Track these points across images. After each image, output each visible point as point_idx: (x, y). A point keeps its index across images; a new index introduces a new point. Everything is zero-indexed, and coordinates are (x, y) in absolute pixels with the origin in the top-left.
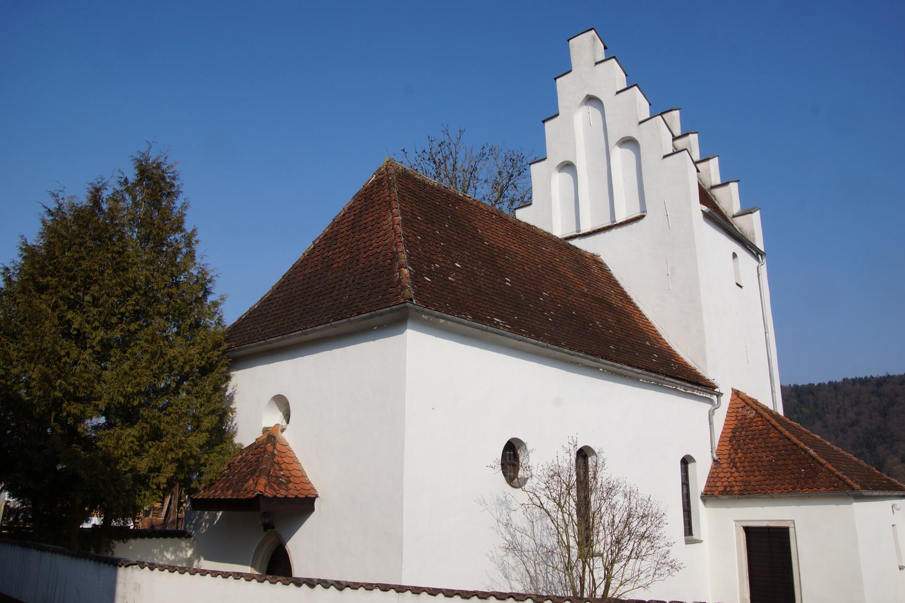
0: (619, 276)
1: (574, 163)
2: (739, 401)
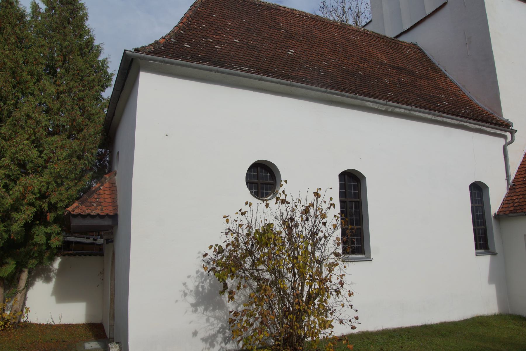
0: (431, 55)
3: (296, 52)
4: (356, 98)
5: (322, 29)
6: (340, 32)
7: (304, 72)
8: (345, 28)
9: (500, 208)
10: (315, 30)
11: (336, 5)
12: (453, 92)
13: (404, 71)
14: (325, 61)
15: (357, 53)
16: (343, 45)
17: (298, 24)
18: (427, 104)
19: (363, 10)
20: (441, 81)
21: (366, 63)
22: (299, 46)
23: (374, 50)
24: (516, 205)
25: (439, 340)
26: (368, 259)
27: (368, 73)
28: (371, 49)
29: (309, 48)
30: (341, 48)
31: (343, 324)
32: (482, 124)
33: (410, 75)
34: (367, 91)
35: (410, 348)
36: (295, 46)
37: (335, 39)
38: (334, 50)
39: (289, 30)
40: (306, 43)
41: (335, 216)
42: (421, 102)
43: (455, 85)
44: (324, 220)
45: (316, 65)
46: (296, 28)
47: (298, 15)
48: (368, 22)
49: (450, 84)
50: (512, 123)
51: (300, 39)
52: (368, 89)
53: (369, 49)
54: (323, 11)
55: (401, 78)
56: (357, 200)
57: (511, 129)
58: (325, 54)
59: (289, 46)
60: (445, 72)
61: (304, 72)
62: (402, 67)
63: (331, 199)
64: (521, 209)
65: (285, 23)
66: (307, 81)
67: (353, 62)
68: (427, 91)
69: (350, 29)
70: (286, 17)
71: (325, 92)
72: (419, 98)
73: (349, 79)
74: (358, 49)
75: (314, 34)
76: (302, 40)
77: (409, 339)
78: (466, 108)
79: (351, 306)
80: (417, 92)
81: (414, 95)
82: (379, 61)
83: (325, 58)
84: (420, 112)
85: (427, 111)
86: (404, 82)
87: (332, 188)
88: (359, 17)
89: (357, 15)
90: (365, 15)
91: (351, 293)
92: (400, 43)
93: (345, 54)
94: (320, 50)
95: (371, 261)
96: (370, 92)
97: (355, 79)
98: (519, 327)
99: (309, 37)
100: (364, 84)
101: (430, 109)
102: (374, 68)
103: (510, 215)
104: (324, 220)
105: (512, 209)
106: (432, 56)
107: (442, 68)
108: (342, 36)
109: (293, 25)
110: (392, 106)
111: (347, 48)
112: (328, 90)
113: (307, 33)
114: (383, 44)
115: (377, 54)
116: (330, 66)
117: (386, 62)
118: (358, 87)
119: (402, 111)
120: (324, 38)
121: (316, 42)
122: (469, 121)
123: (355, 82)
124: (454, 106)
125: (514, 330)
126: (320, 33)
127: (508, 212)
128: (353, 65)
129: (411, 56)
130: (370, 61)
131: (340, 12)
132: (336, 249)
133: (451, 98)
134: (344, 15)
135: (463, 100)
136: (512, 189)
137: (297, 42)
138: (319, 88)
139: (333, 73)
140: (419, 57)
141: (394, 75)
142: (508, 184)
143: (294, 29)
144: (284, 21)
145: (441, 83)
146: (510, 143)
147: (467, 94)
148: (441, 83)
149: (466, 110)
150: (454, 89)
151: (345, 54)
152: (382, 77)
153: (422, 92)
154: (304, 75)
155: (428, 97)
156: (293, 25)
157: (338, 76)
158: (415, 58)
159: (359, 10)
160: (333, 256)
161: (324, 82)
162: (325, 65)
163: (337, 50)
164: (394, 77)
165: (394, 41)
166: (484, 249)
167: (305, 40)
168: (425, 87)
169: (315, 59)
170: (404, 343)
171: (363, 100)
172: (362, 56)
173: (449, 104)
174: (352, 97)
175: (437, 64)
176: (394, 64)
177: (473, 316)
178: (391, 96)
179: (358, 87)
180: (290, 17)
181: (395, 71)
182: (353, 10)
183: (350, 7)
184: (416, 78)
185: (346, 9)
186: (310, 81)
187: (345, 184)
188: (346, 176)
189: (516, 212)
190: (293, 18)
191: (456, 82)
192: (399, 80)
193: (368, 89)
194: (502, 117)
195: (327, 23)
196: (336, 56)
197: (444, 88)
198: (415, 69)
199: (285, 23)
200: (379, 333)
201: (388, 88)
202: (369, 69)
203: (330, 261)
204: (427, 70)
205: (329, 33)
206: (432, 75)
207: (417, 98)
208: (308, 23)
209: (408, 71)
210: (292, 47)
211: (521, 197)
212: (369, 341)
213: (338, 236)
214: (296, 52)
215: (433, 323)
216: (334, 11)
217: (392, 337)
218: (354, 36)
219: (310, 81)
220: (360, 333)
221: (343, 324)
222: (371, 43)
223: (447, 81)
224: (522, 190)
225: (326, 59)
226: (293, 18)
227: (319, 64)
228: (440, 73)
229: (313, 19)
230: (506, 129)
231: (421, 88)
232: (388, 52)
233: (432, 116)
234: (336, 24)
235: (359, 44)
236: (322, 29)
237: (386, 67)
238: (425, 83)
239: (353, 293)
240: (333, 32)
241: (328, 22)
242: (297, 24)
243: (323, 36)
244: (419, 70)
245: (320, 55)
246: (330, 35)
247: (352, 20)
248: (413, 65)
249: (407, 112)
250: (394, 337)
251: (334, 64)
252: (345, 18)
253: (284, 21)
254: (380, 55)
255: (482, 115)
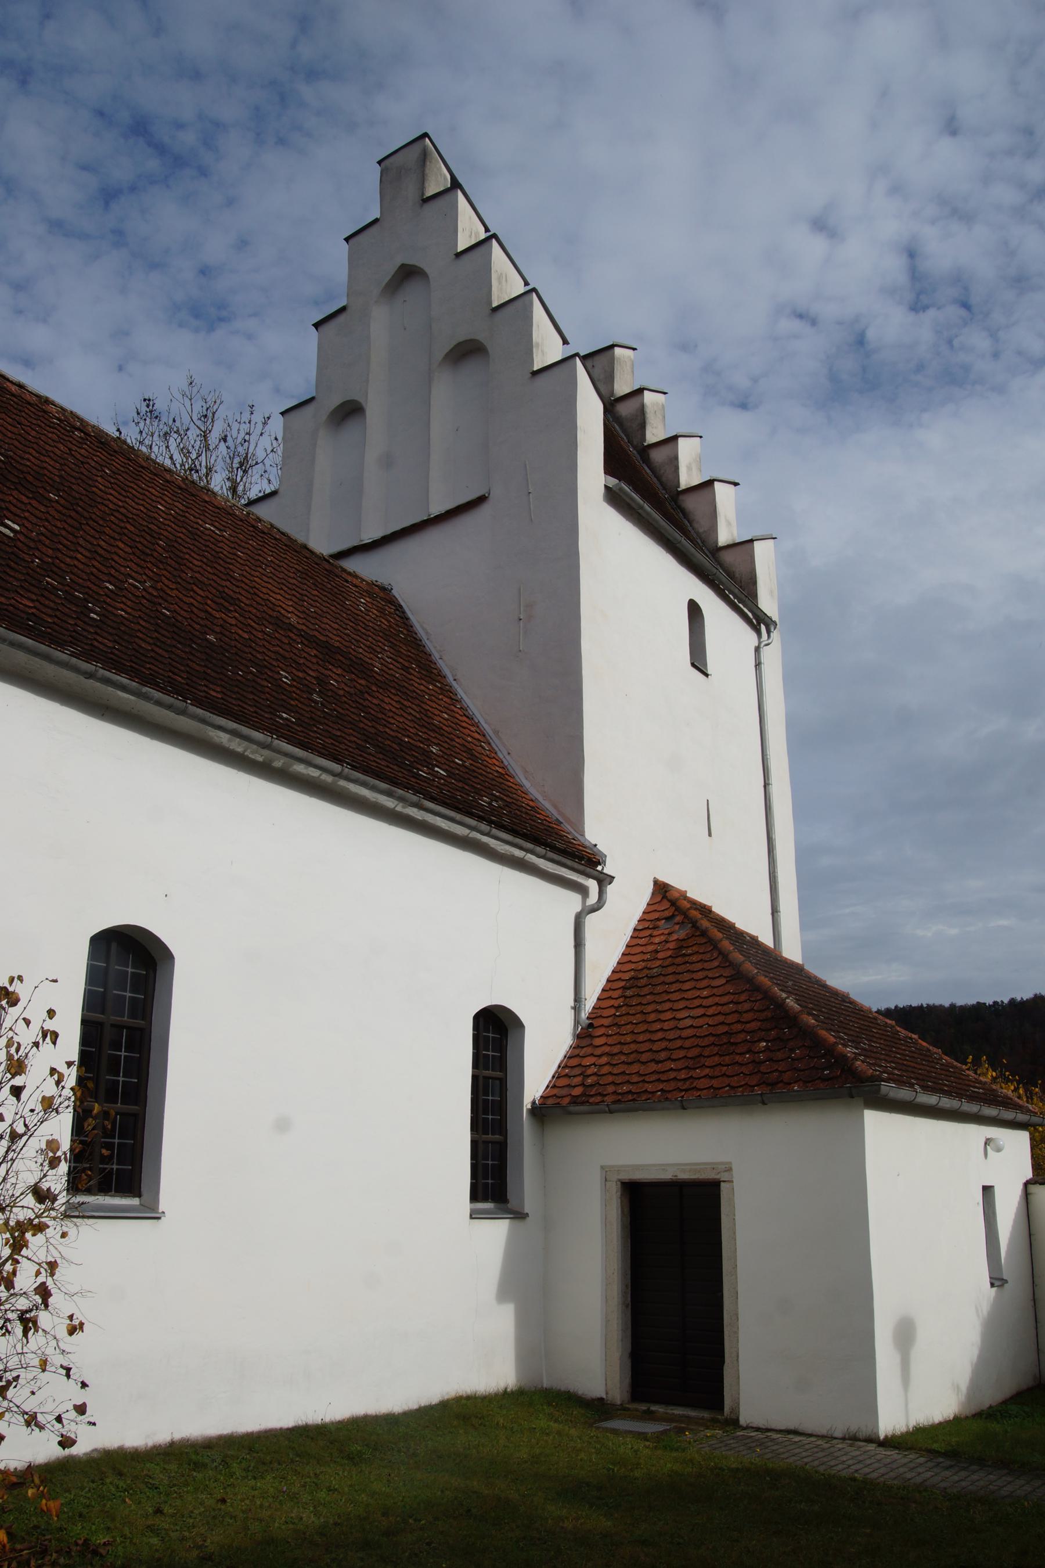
0: (424, 629)
1: (364, 404)
2: (666, 904)
3: (24, 531)
4: (183, 712)
5: (122, 480)
6: (176, 504)
7: (38, 601)
8: (193, 495)
9: (548, 1086)
10: (99, 479)
11: (186, 420)
12: (466, 744)
13: (341, 658)
14: (111, 579)
15: (215, 578)
16: (176, 545)
17: (50, 449)
18: (388, 767)
19: (260, 455)
20: (440, 708)
21: (235, 611)
22: (40, 515)
23: (265, 579)
24: (589, 1081)
25: (341, 1473)
26: (151, 1212)
27: (233, 643)
28: (257, 574)
29: (70, 529)
30: (167, 551)
31: (37, 1425)
32: (530, 846)
33: (356, 672)
34: (220, 696)
35: (247, 1502)
36: (27, 514)
37: (155, 522)
38: (147, 555)
39: (18, 459)
40: (64, 511)
41: (53, 1071)
42: (372, 758)
43: (473, 725)
44: (18, 1081)
45: (79, 584)
46: (42, 458)
47: (58, 419)
48: (268, 491)
49: (460, 718)
50: (606, 856)
51: (46, 495)
52: (225, 690)
53: (253, 573)
54: (142, 425)
55: (327, 676)
56: (140, 1023)
57: (601, 872)
58: (116, 558)
59: (7, 509)
60: (454, 684)
61: (38, 601)
62: (337, 644)
63: (51, 1013)
64: (600, 1094)
65: (9, 435)
66: (42, 631)
67: (195, 602)
68: (394, 727)
69: (206, 502)
70: (17, 418)
71: (90, 675)
72: (369, 744)
73: (174, 649)
74: (219, 567)
75: (94, 489)
76: (50, 500)
77: (250, 1474)
78: (493, 795)
79: (68, 1370)
80: (367, 725)
81: (355, 733)
82: (275, 614)
83: (113, 571)
84: (364, 784)
85: (384, 786)
86: (335, 690)
87: (55, 981)
88: (245, 472)
89: (241, 464)
90: (265, 471)
91: (76, 1322)
92: (344, 575)
93: (175, 573)
94: (102, 543)
95: (159, 1218)
96: (230, 700)
97: (191, 653)
98: (561, 1426)
99: (77, 496)
100: (213, 674)
101: (394, 782)
102: (255, 632)
103: (572, 1108)
104: (18, 1081)
105: (577, 1091)
106: (427, 633)
107: (446, 671)
108: (179, 517)
109: (35, 446)
110: (286, 755)
111: (187, 556)
112: (101, 671)
113: (74, 481)
114: (296, 566)
115: (271, 594)
116: (124, 599)
117: (294, 620)
118: (194, 679)
119: (314, 773)
120: (122, 510)
121: (94, 516)
122: (495, 831)
123: (190, 664)
124: (460, 784)
125: (547, 1434)
126: (113, 492)
127: (567, 1100)
128: (195, 610)
129: (368, 618)
130: (246, 608)
131: (192, 442)
132: (45, 1176)
133: (457, 760)
134: (204, 454)
135: (489, 770)
136: (584, 1036)
137: (34, 502)
138: (74, 660)
139: (127, 623)
140: (390, 626)
141: (310, 665)
142: (577, 1021)
143: (33, 460)
144: (9, 427)
145: (437, 712)
146: (594, 909)
147: (501, 756)
148: (437, 712)
149: (492, 801)
150: (469, 735)
151: (175, 573)
152: (274, 663)
153: (381, 728)
154: (34, 607)
155: (395, 746)
156: (35, 446)
157: (141, 635)
158: (377, 628)
159: (251, 450)
160: (30, 1200)
161: (92, 645)
162: (109, 593)
163: (155, 554)
164: (308, 670)
165: (327, 566)
166: (494, 1200)
167: (62, 502)
168: (391, 714)
169: (81, 566)
170: (233, 1485)
171: (204, 721)
172: (226, 590)
173: (450, 774)
174: (170, 707)
175: (436, 656)
176: (316, 633)
177: (446, 1398)
178: (287, 725)
179: (194, 679)
180: (30, 419)
181: (315, 652)
182: (232, 448)
183: (226, 436)
184: (369, 684)
185: (214, 438)
186: (49, 630)
187: (107, 969)
188: (114, 946)
189: (588, 1102)
190: (39, 426)
191: (479, 717)
192: (322, 682)
193: (225, 690)
194: (583, 835)
195: (143, 467)
196: (147, 571)
197: (444, 727)
198: (371, 659)
199: (9, 435)
200: (159, 1454)
201: (282, 700)
202: (240, 632)
203: (20, 1214)
204: (405, 669)
205: (141, 497)
206: (416, 685)
207: (363, 744)
208: (83, 452)
209: (350, 659)
210: (15, 515)
211: (604, 1060)
212: (121, 1484)
213: (54, 1137)
214: (24, 531)
215: (327, 1420)
216: (175, 436)
217: (198, 1466)
218: (217, 524)
219: (49, 630)
220: (95, 1455)
221: (37, 1425)
222: (259, 555)
223: (455, 709)
224: (610, 1041)
225: (117, 574)
226: (39, 426)
227: (91, 586)
228: (439, 682)
229: (102, 443)
230: (588, 870)
231: (380, 715)
232: (305, 592)
233: (396, 802)
234: (168, 477)
235: (225, 553)
236: (122, 480)
237: (292, 635)
238: (394, 703)
239: (81, 1324)
240: (154, 498)
241: (144, 464)
242: (48, 447)
243: (120, 504)
244: (382, 664)
245: (98, 558)
246: (142, 505)
247: (224, 475)
248: (369, 647)
249: (328, 778)
250: (205, 1466)
251: (138, 593)
252: (204, 464)
253: (9, 427)
254: (279, 597)
255: (534, 821)
